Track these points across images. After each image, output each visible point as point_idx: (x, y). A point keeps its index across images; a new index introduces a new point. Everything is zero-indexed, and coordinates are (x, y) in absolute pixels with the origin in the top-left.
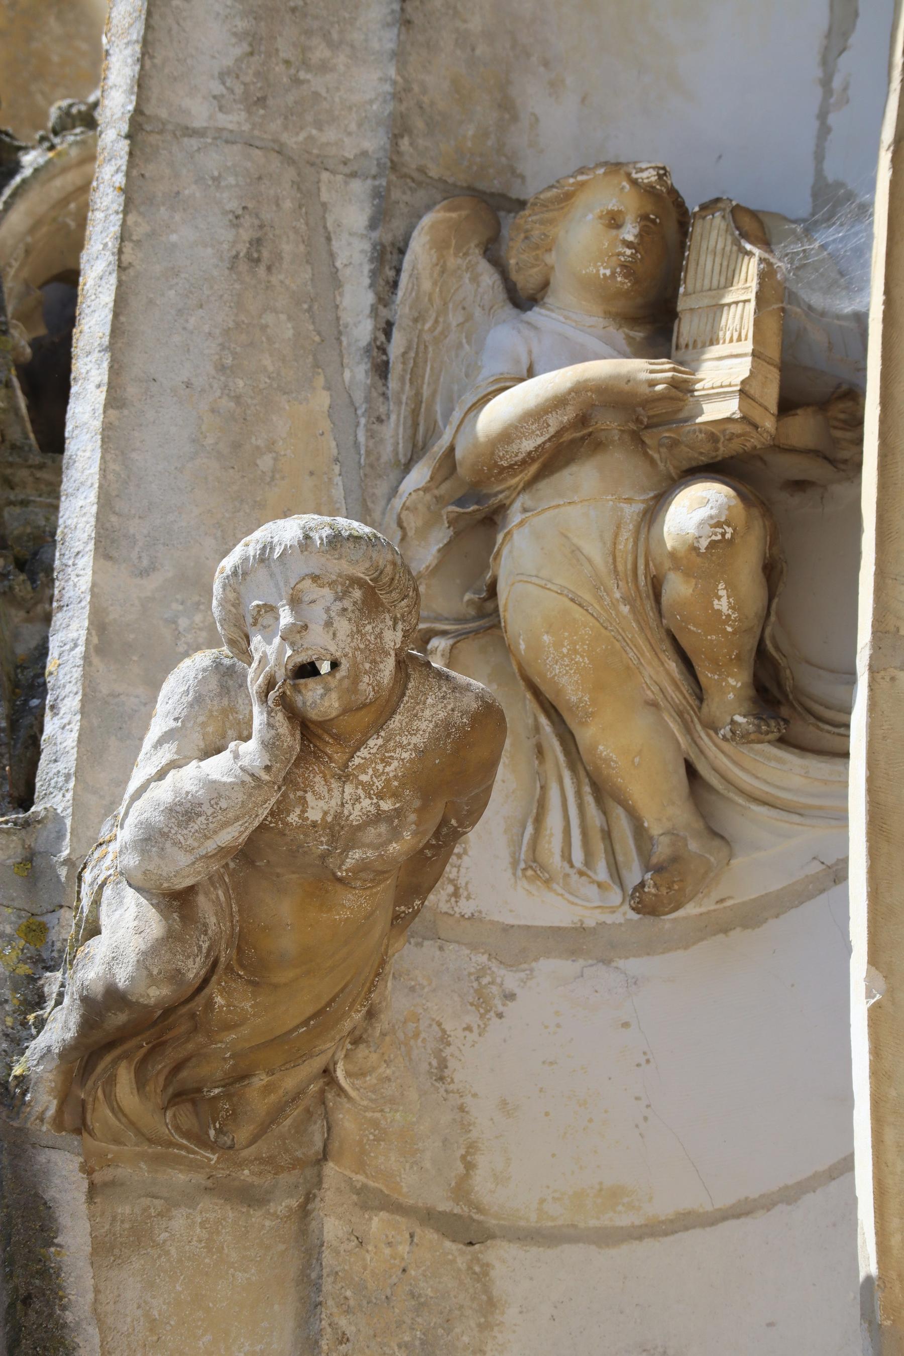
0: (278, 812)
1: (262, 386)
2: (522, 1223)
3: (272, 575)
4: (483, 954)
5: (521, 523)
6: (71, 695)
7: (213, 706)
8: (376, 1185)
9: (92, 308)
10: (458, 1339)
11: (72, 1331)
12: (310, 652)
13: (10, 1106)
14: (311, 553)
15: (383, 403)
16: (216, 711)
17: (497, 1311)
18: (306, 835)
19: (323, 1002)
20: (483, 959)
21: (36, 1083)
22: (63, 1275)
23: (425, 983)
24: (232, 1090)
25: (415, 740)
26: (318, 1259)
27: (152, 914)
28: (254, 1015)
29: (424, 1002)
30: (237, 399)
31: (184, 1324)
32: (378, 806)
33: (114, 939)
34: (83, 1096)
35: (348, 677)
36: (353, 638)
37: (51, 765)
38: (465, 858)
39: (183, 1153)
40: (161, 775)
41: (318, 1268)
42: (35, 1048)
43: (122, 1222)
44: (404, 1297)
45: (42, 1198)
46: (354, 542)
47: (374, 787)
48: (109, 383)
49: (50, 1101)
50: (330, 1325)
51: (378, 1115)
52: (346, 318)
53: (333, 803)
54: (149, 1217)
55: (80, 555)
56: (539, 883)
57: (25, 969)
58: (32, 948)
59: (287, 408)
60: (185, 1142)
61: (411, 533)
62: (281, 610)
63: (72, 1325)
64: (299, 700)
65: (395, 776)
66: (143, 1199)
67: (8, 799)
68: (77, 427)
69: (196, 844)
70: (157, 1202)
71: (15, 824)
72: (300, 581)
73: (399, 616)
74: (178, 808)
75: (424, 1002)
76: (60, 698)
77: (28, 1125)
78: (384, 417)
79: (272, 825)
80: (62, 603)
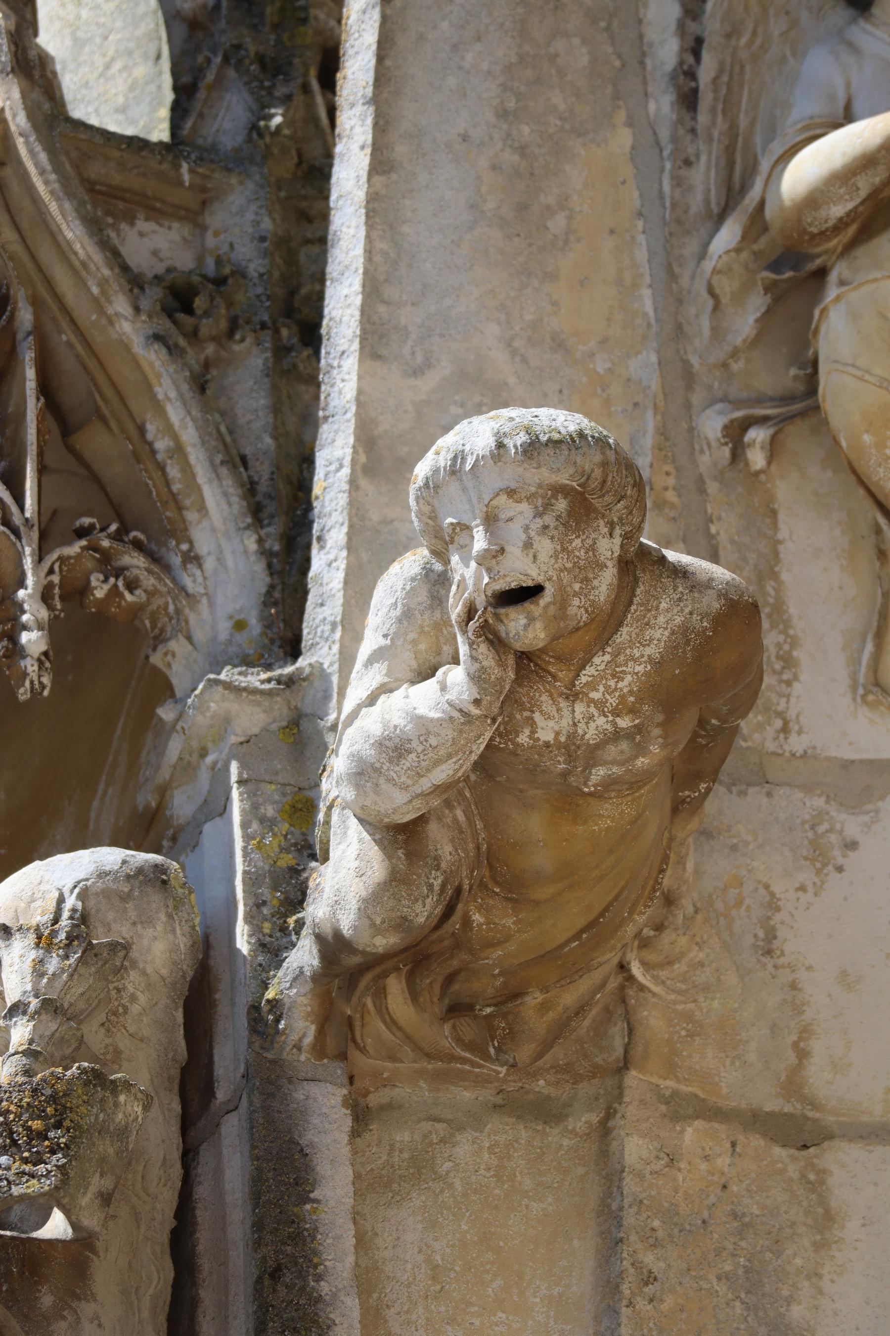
0: (507, 732)
1: (551, 130)
2: (865, 1118)
3: (464, 490)
4: (820, 796)
5: (838, 299)
6: (338, 526)
7: (423, 620)
8: (690, 1089)
9: (355, 49)
10: (789, 1263)
11: (327, 1305)
12: (508, 579)
13: (264, 1033)
14: (505, 463)
15: (692, 141)
16: (428, 626)
17: (836, 1226)
18: (540, 755)
19: (595, 913)
20: (819, 802)
21: (290, 1008)
22: (319, 1237)
23: (750, 838)
24: (504, 1009)
25: (648, 651)
26: (619, 1187)
27: (375, 852)
28: (518, 931)
29: (749, 861)
30: (522, 150)
31: (470, 1269)
32: (614, 724)
33: (336, 879)
34: (349, 1012)
35: (553, 603)
36: (557, 558)
37: (318, 610)
38: (796, 686)
39: (467, 1067)
40: (371, 700)
41: (619, 1198)
42: (288, 968)
43: (401, 1151)
44: (724, 1219)
45: (298, 1144)
46: (554, 447)
47: (608, 705)
48: (374, 144)
49: (306, 1027)
50: (633, 1264)
51: (691, 1006)
52: (651, 34)
53: (564, 723)
54: (431, 1144)
55: (346, 355)
56: (882, 708)
57: (287, 860)
58: (297, 832)
59: (583, 153)
60: (467, 1055)
61: (725, 300)
62: (475, 530)
63: (328, 1297)
64: (502, 629)
65: (630, 691)
66: (423, 1124)
67: (278, 643)
68: (341, 196)
69: (409, 782)
70: (439, 1126)
71: (279, 682)
72: (494, 498)
73: (616, 519)
74: (387, 743)
75: (749, 861)
76: (327, 528)
77: (284, 1055)
78: (692, 158)
79: (502, 746)
80: (327, 413)
